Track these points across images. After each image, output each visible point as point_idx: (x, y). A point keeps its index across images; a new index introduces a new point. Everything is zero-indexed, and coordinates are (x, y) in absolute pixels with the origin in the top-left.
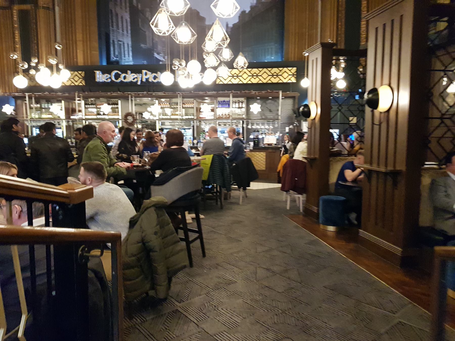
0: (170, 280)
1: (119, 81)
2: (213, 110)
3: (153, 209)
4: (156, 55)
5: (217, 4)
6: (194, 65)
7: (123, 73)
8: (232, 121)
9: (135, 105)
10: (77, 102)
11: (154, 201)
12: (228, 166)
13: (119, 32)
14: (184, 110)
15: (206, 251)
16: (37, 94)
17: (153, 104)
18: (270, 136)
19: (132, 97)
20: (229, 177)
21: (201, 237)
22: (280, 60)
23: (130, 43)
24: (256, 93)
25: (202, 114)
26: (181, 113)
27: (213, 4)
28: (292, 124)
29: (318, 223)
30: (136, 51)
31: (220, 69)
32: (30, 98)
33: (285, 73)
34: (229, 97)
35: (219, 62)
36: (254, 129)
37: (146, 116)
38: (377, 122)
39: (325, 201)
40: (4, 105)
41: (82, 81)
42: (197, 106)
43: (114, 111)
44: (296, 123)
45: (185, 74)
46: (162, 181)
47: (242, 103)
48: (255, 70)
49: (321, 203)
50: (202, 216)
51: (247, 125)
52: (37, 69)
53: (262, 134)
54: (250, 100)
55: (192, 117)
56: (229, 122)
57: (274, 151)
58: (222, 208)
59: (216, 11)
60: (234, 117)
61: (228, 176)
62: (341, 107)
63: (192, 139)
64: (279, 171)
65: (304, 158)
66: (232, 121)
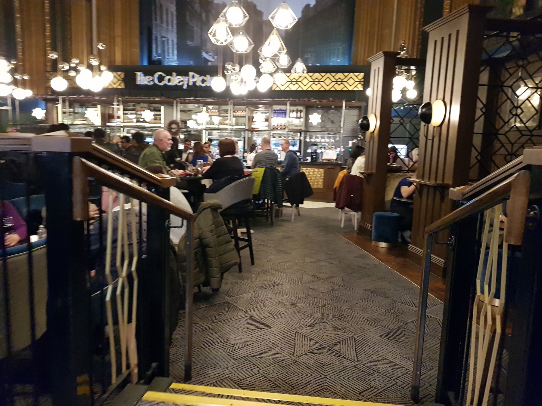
0: (222, 274)
1: (162, 84)
2: (267, 120)
3: (209, 210)
4: (204, 54)
5: (275, 16)
6: (249, 69)
7: (167, 75)
8: (288, 133)
9: (181, 111)
10: (115, 107)
11: (210, 203)
12: (280, 180)
13: (163, 26)
14: (234, 119)
15: (255, 261)
16: (72, 97)
17: (200, 112)
18: (330, 151)
19: (177, 103)
20: (281, 194)
21: (250, 246)
22: (347, 64)
23: (175, 40)
24: (316, 101)
25: (254, 124)
26: (231, 122)
27: (271, 16)
28: (356, 137)
29: (371, 241)
30: (182, 49)
31: (275, 75)
32: (64, 101)
33: (351, 79)
34: (286, 105)
35: (276, 68)
36: (313, 142)
37: (191, 124)
38: (430, 136)
39: (378, 217)
40: (34, 109)
41: (121, 83)
42: (249, 115)
43: (157, 118)
44: (360, 136)
45: (238, 79)
46: (214, 190)
47: (301, 112)
48: (317, 75)
49: (374, 218)
50: (252, 231)
51: (305, 137)
52: (75, 69)
53: (321, 148)
54: (310, 109)
55: (244, 127)
56: (285, 134)
57: (333, 167)
58: (272, 224)
59: (274, 23)
60: (290, 128)
61: (281, 193)
62: (403, 120)
63: (242, 152)
64: (336, 188)
65: (360, 173)
66: (288, 133)
